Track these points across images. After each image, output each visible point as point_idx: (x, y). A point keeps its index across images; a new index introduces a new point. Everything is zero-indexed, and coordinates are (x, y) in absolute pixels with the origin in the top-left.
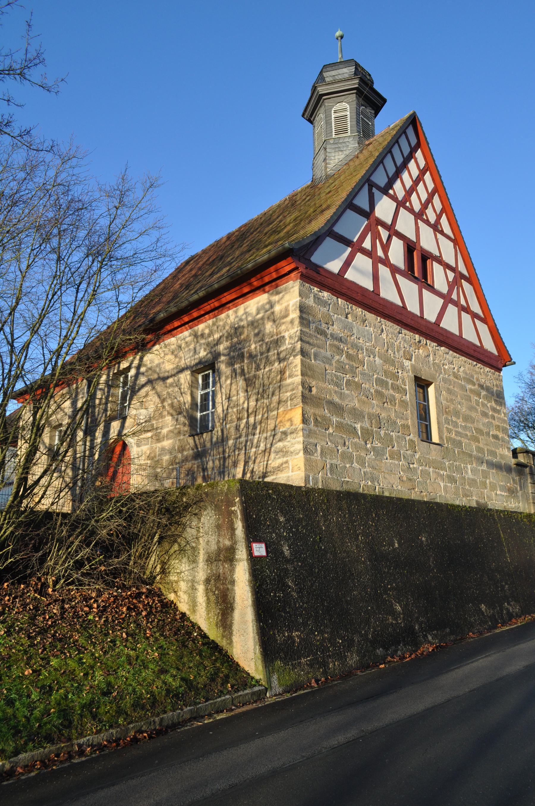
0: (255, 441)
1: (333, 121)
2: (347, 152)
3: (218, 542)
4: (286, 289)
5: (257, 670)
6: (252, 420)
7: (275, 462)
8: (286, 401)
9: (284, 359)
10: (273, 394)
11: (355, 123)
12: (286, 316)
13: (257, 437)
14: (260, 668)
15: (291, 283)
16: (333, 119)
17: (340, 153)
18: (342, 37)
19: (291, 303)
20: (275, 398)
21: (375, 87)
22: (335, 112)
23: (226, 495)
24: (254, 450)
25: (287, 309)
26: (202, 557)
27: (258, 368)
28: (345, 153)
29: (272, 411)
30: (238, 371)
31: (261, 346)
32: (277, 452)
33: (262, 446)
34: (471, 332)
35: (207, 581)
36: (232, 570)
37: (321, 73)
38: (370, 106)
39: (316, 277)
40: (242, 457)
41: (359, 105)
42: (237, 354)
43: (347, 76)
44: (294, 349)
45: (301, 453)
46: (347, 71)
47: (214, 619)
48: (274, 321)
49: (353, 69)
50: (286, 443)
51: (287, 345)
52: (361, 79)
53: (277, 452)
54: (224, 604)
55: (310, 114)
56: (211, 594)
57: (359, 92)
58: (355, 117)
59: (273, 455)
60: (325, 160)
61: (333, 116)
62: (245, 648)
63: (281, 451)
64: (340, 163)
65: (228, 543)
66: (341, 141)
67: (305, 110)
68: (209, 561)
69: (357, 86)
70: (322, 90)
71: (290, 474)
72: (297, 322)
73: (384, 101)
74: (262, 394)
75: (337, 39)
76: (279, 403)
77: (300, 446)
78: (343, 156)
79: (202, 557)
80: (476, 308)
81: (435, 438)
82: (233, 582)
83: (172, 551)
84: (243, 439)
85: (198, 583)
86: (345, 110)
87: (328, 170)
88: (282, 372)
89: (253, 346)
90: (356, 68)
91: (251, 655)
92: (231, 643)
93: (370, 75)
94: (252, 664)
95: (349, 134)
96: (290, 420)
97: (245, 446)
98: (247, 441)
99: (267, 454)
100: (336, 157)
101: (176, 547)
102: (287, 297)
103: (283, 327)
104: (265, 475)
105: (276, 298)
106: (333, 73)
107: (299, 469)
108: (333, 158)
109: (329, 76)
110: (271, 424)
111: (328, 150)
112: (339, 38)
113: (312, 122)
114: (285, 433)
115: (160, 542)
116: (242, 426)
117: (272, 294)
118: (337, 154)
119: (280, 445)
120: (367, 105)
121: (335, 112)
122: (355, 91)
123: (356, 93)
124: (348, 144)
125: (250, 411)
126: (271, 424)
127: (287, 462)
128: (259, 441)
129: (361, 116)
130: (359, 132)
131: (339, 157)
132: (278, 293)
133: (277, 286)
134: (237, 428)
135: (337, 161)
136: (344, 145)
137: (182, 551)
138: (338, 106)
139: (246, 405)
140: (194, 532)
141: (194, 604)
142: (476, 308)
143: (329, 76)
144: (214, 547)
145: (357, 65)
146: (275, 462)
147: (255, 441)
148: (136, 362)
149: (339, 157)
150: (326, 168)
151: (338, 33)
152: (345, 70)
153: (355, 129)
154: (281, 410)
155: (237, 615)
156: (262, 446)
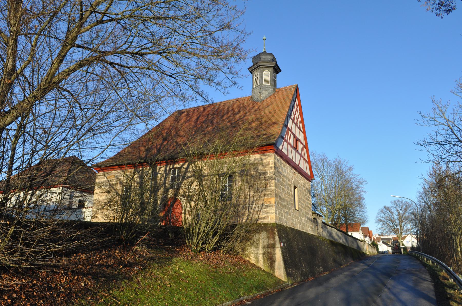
0: (253, 207)
2: (269, 92)
3: (268, 242)
4: (268, 155)
5: (285, 279)
6: (252, 200)
7: (262, 215)
8: (268, 195)
9: (267, 180)
10: (262, 191)
12: (269, 165)
13: (254, 205)
14: (286, 278)
15: (270, 153)
19: (271, 161)
20: (263, 193)
22: (265, 74)
23: (271, 227)
24: (252, 210)
25: (269, 163)
26: (261, 246)
27: (255, 181)
29: (261, 197)
30: (245, 180)
31: (256, 173)
32: (263, 212)
33: (257, 209)
34: (305, 167)
35: (264, 254)
36: (274, 251)
39: (279, 153)
40: (247, 212)
42: (243, 173)
44: (272, 177)
45: (274, 214)
46: (270, 58)
47: (267, 265)
48: (263, 165)
49: (272, 58)
50: (268, 209)
51: (269, 175)
53: (263, 212)
54: (271, 261)
56: (265, 258)
57: (274, 68)
59: (261, 213)
62: (280, 272)
63: (265, 212)
65: (272, 242)
67: (250, 68)
68: (264, 247)
70: (260, 64)
71: (269, 220)
72: (273, 168)
73: (281, 71)
74: (257, 190)
76: (265, 195)
77: (274, 211)
79: (261, 246)
80: (306, 159)
81: (297, 208)
82: (275, 254)
83: (247, 244)
84: (247, 206)
85: (260, 254)
86: (268, 74)
88: (266, 185)
89: (252, 173)
91: (283, 275)
92: (274, 272)
94: (283, 277)
96: (270, 202)
97: (249, 208)
98: (249, 207)
99: (259, 212)
101: (249, 243)
102: (269, 158)
103: (267, 169)
104: (258, 220)
105: (264, 157)
107: (273, 219)
109: (263, 57)
110: (261, 202)
113: (252, 73)
114: (267, 206)
115: (241, 241)
116: (247, 201)
117: (262, 155)
119: (265, 210)
121: (265, 74)
125: (251, 196)
126: (261, 202)
127: (268, 216)
128: (255, 207)
132: (264, 156)
133: (264, 153)
134: (244, 201)
137: (252, 244)
139: (249, 194)
140: (257, 238)
141: (258, 261)
142: (306, 159)
144: (266, 243)
146: (262, 215)
147: (253, 207)
148: (185, 166)
150: (260, 96)
151: (264, 38)
152: (269, 57)
154: (266, 198)
155: (276, 264)
156: (257, 209)
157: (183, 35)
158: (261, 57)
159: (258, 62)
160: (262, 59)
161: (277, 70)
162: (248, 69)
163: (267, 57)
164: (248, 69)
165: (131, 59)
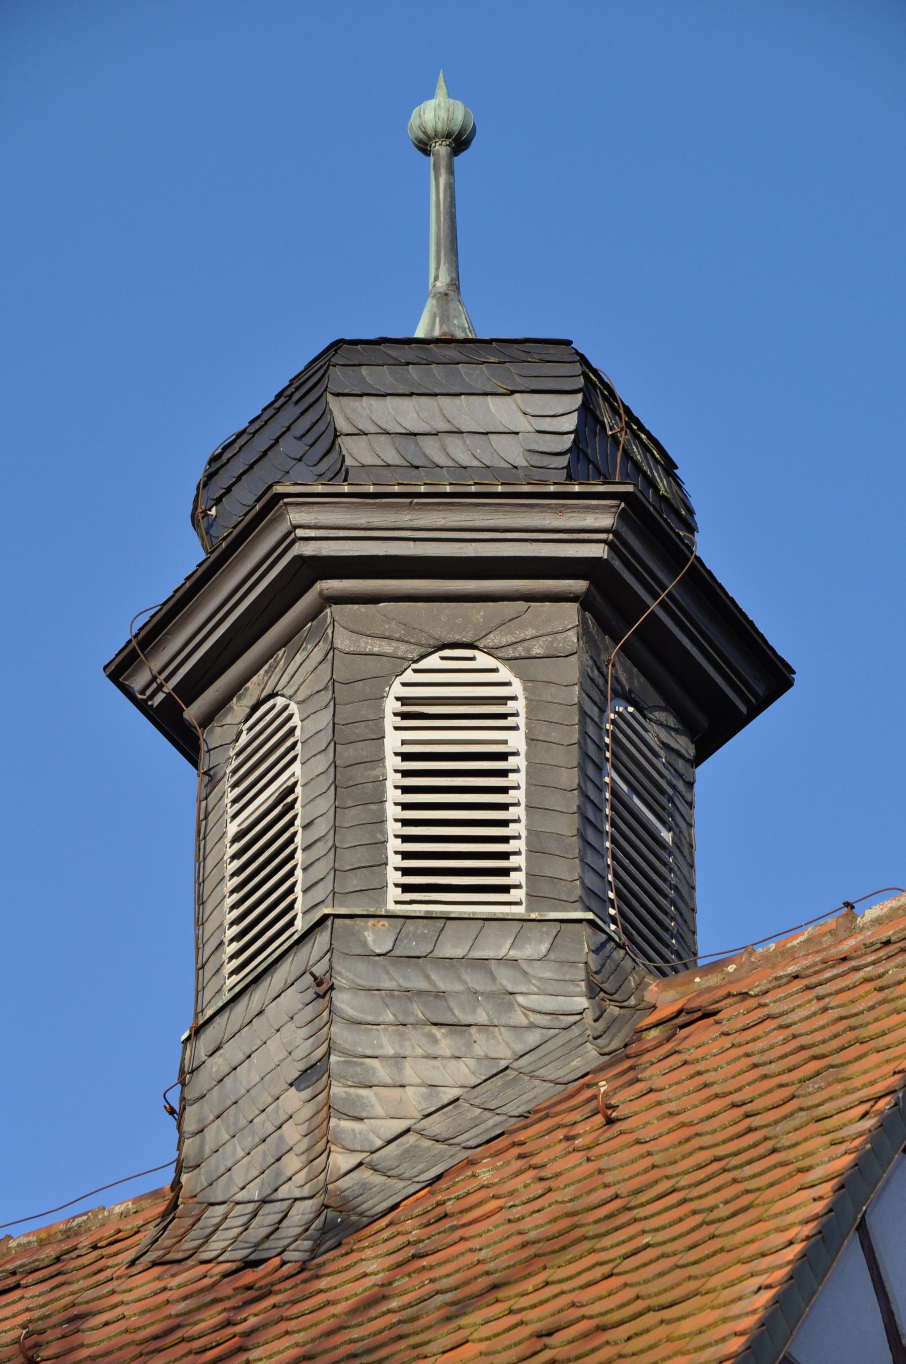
1: (393, 779)
2: (502, 1047)
11: (567, 826)
16: (392, 762)
17: (446, 1043)
18: (460, 142)
21: (710, 548)
28: (482, 1045)
37: (307, 389)
38: (671, 705)
41: (597, 689)
43: (512, 453)
46: (527, 425)
49: (563, 414)
52: (634, 511)
55: (178, 682)
57: (606, 597)
58: (570, 778)
60: (312, 1074)
61: (393, 741)
64: (437, 1125)
66: (451, 948)
67: (151, 637)
69: (598, 551)
70: (318, 527)
75: (424, 147)
78: (464, 1072)
86: (492, 709)
87: (341, 1161)
90: (587, 411)
93: (669, 467)
95: (517, 903)
100: (409, 1073)
106: (408, 413)
108: (382, 1071)
109: (373, 423)
111: (343, 1001)
112: (441, 149)
113: (188, 742)
118: (415, 1043)
120: (652, 697)
122: (579, 586)
123: (584, 602)
124: (506, 979)
129: (610, 776)
130: (592, 898)
131: (434, 1072)
135: (414, 1100)
136: (476, 981)
138: (434, 675)
143: (373, 423)
145: (596, 392)
149: (434, 1072)
150: (321, 1140)
151: (436, 112)
152: (503, 411)
153: (568, 870)
157: (666, 1149)
158: (344, 413)
159: (271, 505)
160: (356, 452)
161: (682, 656)
162: (119, 672)
163: (467, 412)
164: (119, 672)
165: (339, 1204)
